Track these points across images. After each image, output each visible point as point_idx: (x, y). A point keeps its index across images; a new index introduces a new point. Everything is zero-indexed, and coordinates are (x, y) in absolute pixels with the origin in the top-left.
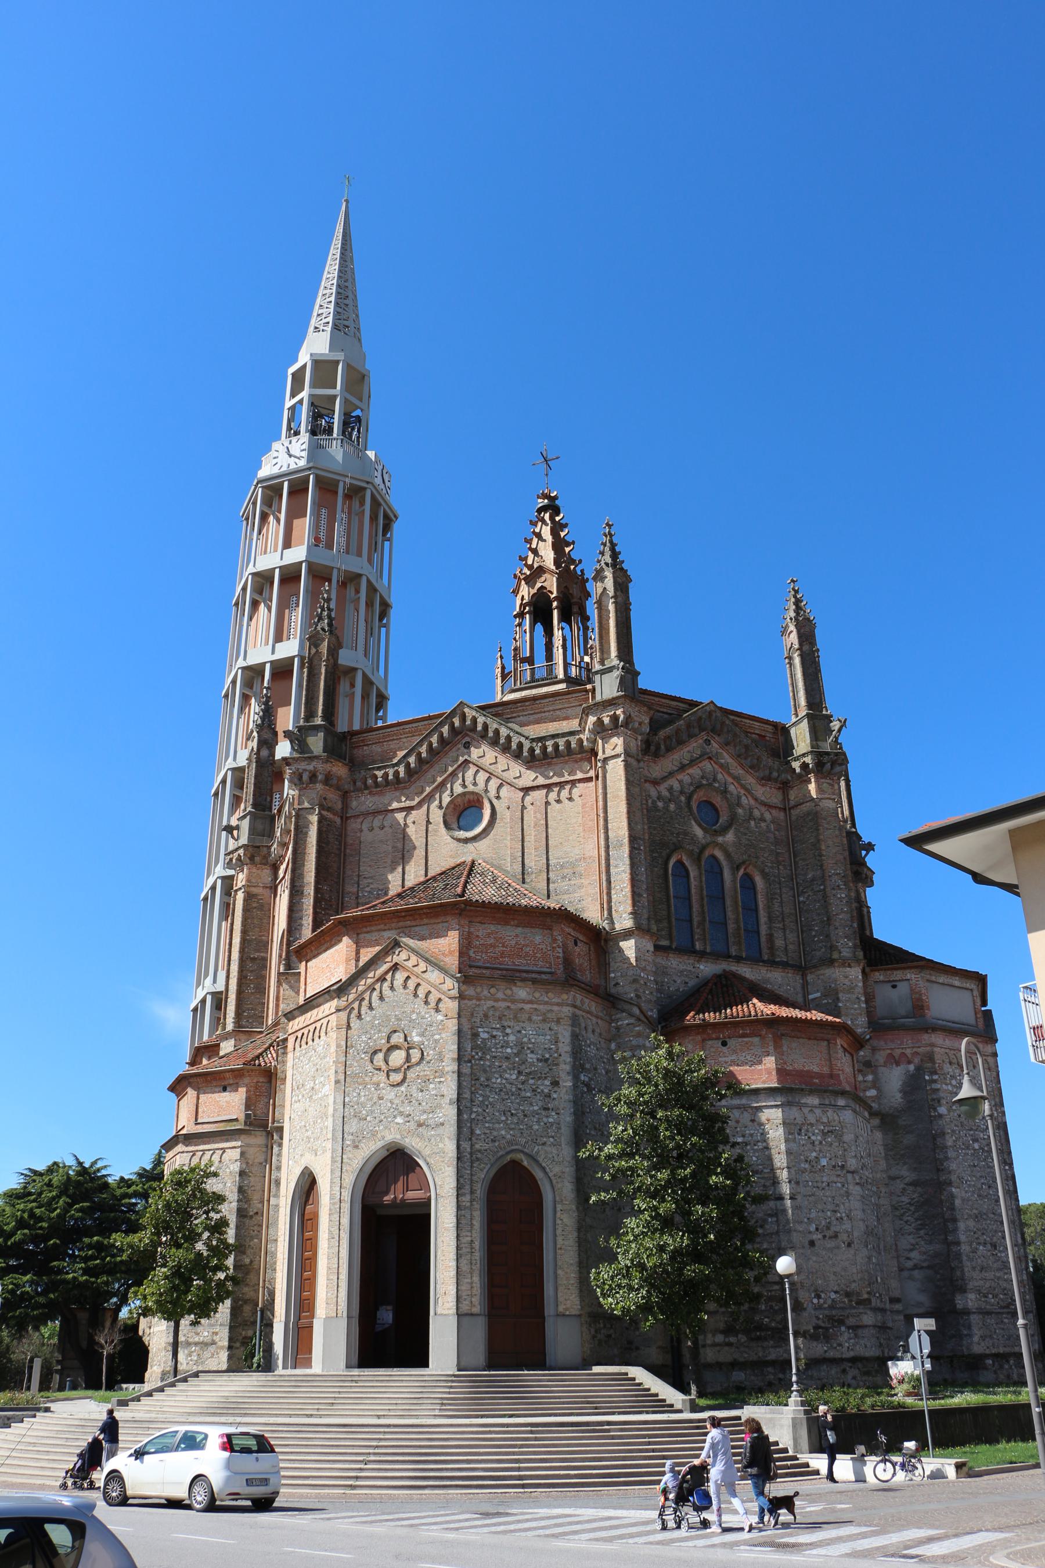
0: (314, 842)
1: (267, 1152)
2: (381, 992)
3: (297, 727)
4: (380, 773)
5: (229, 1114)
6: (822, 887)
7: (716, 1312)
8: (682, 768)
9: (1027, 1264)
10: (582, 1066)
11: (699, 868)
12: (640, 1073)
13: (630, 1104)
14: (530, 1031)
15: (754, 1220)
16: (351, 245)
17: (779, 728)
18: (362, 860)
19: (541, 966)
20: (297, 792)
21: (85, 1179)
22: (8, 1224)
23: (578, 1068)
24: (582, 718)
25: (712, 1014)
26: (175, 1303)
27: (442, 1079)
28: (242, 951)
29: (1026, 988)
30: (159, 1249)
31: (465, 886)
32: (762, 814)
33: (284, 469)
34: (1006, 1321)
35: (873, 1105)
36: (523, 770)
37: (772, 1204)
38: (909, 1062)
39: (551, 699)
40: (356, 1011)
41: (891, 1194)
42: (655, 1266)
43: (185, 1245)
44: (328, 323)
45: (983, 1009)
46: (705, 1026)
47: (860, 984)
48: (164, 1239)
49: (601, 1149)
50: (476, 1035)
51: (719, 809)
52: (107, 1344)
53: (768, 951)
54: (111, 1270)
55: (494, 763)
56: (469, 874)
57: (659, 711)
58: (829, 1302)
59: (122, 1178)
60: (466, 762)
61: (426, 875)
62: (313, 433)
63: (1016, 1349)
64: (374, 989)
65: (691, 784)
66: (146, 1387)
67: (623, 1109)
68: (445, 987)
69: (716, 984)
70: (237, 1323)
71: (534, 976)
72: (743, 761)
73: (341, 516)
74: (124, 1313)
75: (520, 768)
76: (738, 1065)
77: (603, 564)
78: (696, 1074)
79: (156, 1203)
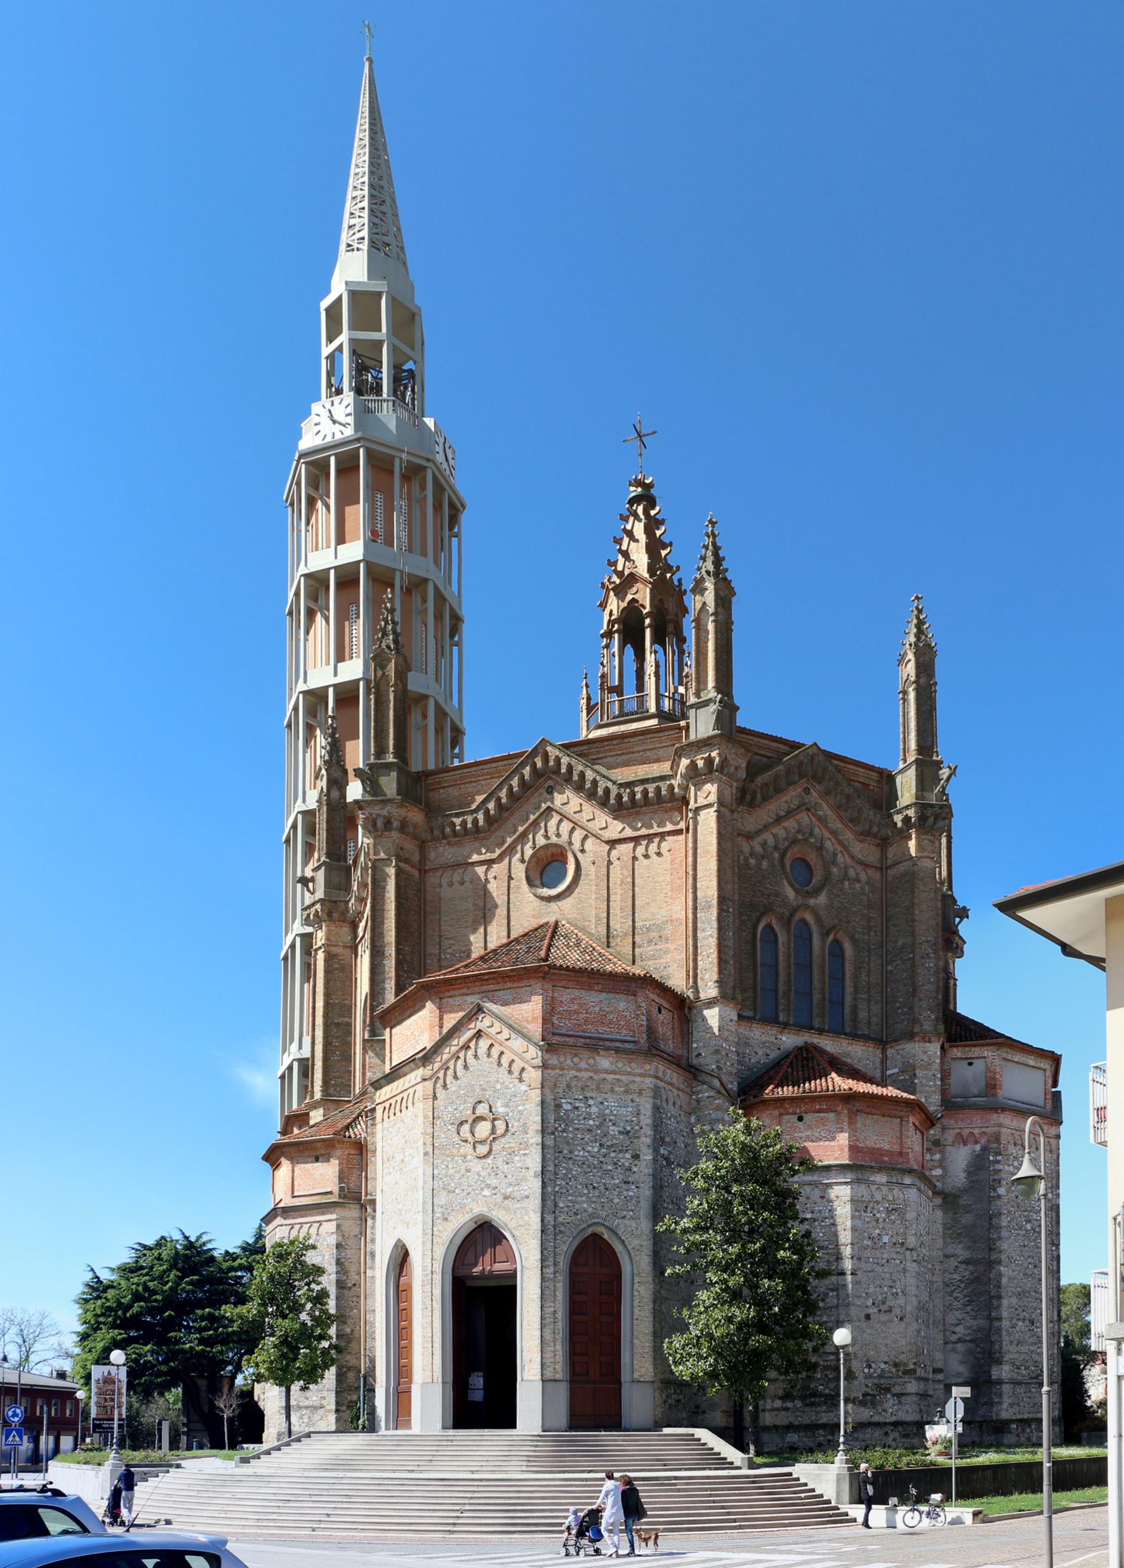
0: (393, 898)
1: (361, 1225)
2: (465, 1061)
3: (367, 765)
4: (458, 821)
5: (324, 1187)
6: (911, 956)
7: (776, 1380)
8: (779, 820)
9: (1059, 1338)
10: (662, 1139)
11: (789, 933)
12: (718, 1147)
13: (706, 1178)
14: (612, 1102)
15: (816, 1295)
16: (382, 126)
17: (885, 775)
18: (443, 918)
19: (625, 1034)
20: (372, 840)
21: (192, 1252)
22: (125, 1297)
23: (659, 1140)
24: (674, 760)
25: (790, 1088)
26: (285, 1370)
27: (527, 1152)
28: (326, 1015)
29: (1097, 1067)
30: (267, 1320)
31: (548, 950)
32: (857, 874)
33: (329, 439)
34: (1033, 1390)
35: (937, 1184)
36: (610, 820)
37: (834, 1279)
38: (976, 1142)
39: (641, 738)
40: (441, 1081)
41: (945, 1271)
42: (722, 1336)
43: (291, 1315)
44: (363, 238)
45: (1053, 1090)
46: (782, 1101)
47: (938, 1061)
48: (270, 1310)
49: (677, 1223)
50: (558, 1106)
51: (814, 868)
52: (227, 1408)
53: (851, 1024)
54: (225, 1340)
55: (579, 812)
56: (553, 936)
57: (756, 754)
58: (879, 1371)
59: (227, 1252)
60: (549, 809)
61: (509, 937)
62: (359, 391)
63: (1039, 1416)
64: (458, 1057)
65: (786, 839)
66: (265, 1446)
67: (700, 1183)
68: (528, 1056)
69: (796, 1056)
70: (342, 1388)
71: (617, 1044)
72: (842, 814)
73: (399, 503)
74: (239, 1380)
75: (607, 818)
76: (812, 1141)
77: (704, 573)
78: (771, 1149)
79: (261, 1275)
